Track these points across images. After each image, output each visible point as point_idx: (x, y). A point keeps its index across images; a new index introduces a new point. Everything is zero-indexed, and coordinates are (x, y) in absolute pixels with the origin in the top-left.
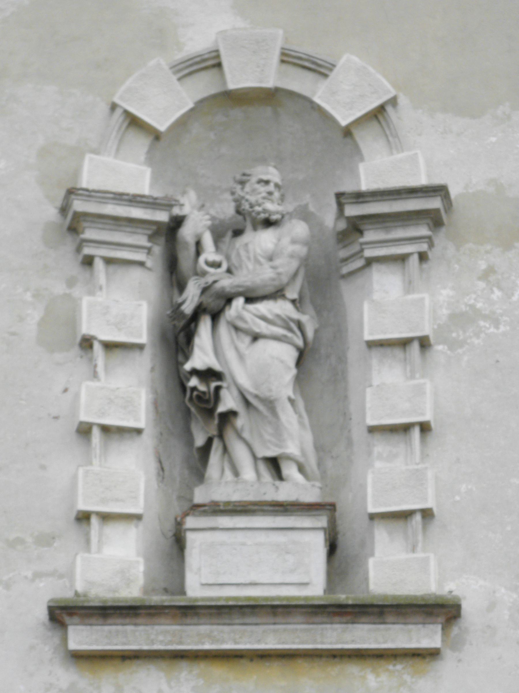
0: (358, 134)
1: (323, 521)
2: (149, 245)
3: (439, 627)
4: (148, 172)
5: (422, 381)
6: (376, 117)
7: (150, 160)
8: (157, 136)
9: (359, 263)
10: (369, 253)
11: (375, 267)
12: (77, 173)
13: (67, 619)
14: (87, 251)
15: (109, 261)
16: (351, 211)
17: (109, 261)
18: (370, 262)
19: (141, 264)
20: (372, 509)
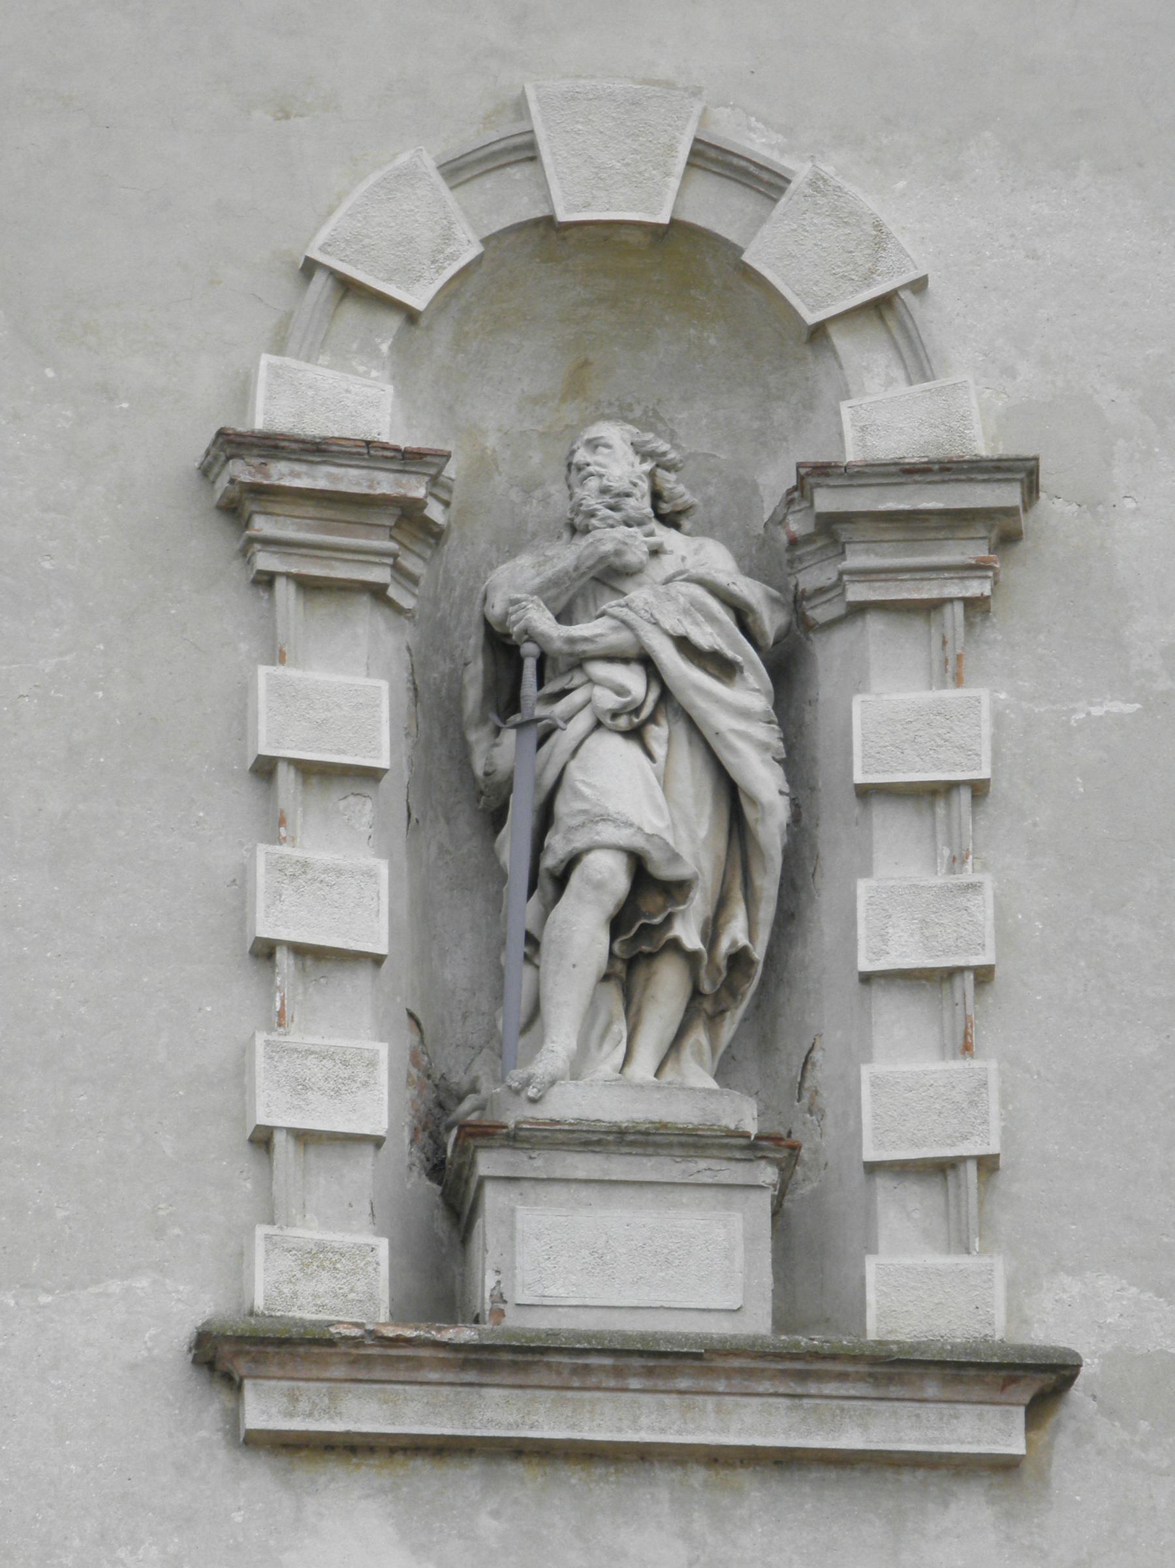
0: (841, 341)
1: (768, 1174)
2: (392, 546)
3: (1019, 1413)
4: (387, 392)
5: (985, 1260)
6: (876, 307)
7: (403, 380)
8: (411, 316)
9: (837, 610)
10: (857, 593)
11: (874, 625)
12: (243, 394)
13: (241, 1367)
14: (265, 561)
15: (308, 586)
16: (826, 501)
17: (308, 586)
18: (859, 610)
19: (378, 593)
20: (870, 1154)
